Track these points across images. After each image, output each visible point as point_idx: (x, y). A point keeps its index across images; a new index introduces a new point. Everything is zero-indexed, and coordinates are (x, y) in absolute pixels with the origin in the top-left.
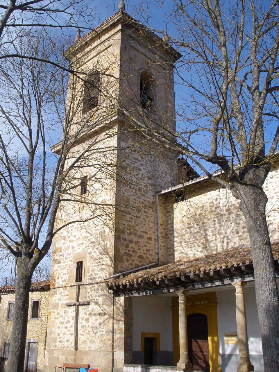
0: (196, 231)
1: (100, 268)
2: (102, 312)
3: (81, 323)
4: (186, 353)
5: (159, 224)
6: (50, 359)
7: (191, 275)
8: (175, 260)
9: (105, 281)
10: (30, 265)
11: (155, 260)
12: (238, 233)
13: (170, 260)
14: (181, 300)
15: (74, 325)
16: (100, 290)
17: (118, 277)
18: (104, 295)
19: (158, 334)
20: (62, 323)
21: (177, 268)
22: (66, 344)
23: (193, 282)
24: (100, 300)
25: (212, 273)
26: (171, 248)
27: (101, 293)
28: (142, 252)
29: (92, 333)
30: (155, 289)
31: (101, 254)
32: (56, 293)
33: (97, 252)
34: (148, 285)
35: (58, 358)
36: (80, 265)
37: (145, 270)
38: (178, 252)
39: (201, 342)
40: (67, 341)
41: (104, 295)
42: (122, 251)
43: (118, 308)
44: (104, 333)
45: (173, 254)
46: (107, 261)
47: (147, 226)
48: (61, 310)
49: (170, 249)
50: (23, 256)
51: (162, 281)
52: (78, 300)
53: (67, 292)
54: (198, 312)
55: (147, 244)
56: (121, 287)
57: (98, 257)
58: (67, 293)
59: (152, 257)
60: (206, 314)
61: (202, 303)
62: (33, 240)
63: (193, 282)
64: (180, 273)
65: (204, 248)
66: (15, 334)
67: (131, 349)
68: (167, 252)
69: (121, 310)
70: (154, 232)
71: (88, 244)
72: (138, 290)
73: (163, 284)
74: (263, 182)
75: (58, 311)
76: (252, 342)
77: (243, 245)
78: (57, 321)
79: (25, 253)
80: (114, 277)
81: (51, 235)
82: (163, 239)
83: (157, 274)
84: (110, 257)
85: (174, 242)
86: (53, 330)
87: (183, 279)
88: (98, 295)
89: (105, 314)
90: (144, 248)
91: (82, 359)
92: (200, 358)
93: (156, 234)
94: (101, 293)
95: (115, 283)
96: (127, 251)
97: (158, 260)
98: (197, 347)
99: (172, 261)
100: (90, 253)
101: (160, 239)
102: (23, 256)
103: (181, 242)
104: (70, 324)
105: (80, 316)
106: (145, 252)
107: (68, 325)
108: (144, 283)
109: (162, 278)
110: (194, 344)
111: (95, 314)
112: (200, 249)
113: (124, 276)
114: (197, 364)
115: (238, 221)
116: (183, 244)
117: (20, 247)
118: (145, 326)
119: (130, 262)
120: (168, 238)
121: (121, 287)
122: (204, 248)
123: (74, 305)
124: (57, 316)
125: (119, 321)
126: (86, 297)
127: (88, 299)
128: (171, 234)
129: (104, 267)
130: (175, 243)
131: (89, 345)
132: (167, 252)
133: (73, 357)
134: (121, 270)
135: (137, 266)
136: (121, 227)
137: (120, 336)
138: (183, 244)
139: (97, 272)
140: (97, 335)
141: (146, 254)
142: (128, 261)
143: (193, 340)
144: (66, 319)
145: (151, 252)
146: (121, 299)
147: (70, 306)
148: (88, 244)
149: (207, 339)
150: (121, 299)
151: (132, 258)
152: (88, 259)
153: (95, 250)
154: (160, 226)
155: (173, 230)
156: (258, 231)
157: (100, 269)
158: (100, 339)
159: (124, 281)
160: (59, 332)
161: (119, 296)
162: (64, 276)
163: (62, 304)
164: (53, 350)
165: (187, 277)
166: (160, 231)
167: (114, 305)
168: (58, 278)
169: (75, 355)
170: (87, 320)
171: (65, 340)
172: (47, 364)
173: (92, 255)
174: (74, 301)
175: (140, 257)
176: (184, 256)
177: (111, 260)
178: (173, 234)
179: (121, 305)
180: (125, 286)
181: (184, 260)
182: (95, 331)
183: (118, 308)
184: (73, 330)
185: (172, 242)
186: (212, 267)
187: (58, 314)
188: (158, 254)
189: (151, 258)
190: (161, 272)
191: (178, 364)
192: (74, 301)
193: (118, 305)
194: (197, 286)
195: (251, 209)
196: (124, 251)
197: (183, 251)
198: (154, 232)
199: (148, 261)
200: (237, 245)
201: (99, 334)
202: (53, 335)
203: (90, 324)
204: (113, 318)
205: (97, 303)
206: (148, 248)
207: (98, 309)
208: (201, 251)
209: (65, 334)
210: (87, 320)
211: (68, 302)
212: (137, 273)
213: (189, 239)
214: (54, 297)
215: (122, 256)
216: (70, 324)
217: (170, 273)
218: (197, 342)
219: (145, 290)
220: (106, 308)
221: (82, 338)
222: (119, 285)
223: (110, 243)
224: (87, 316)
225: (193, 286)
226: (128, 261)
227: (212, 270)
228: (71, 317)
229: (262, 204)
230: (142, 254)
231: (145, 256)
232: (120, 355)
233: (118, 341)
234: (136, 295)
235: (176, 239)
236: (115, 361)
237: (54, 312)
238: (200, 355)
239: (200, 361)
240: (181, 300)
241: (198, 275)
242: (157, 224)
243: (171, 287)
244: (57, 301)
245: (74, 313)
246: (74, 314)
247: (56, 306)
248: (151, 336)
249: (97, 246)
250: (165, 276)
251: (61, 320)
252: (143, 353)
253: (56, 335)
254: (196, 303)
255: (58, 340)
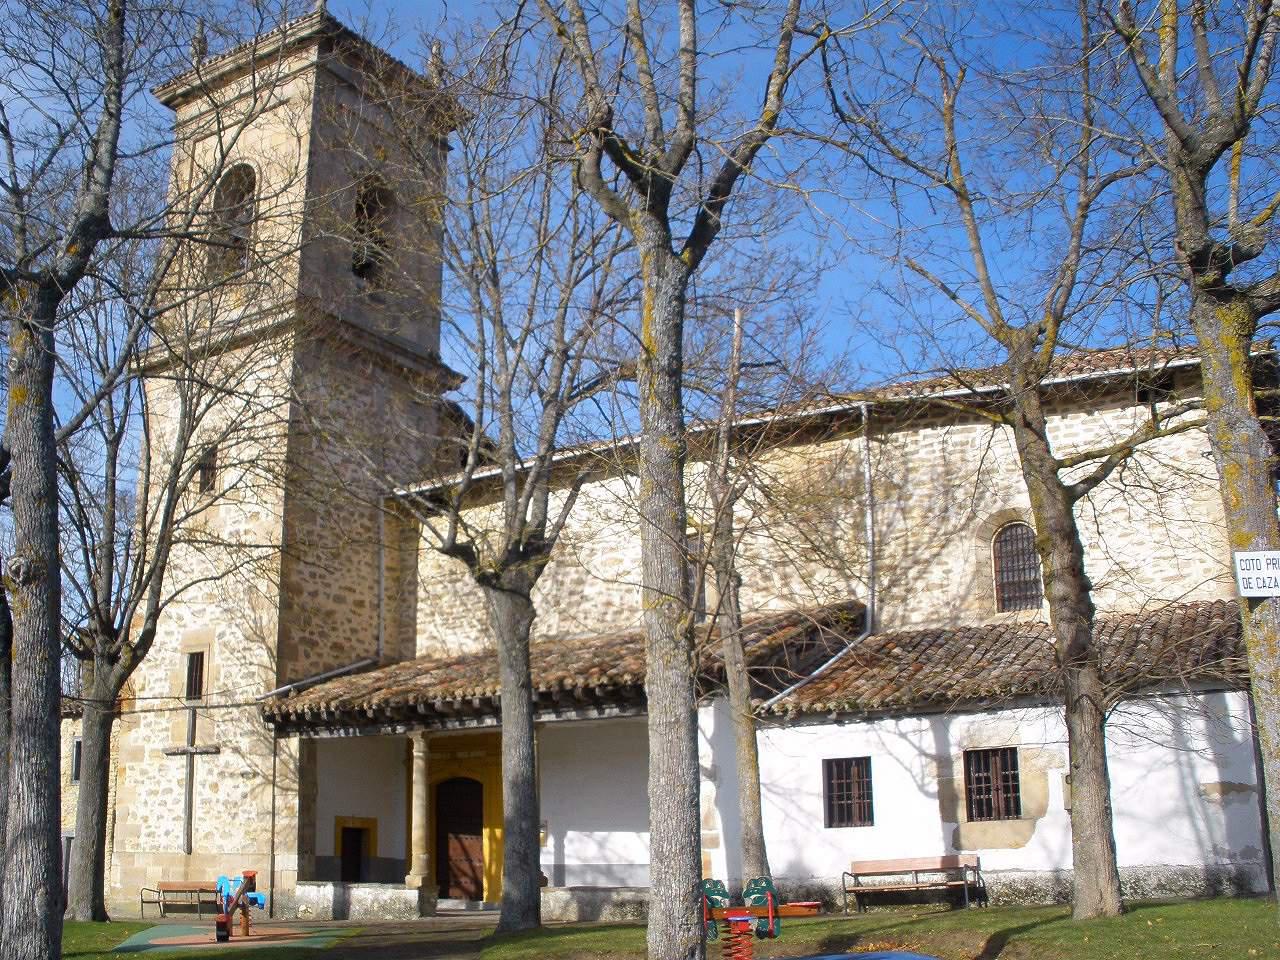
0: (467, 590)
1: (245, 671)
2: (248, 769)
3: (201, 794)
4: (423, 857)
5: (383, 567)
6: (125, 873)
7: (438, 703)
8: (418, 654)
9: (260, 704)
10: (113, 680)
11: (371, 654)
12: (557, 603)
13: (405, 653)
14: (418, 751)
15: (183, 798)
16: (244, 720)
17: (286, 694)
18: (253, 733)
19: (375, 821)
20: (155, 793)
21: (412, 682)
22: (163, 841)
23: (442, 716)
24: (245, 743)
25: (476, 702)
26: (409, 625)
27: (248, 727)
28: (341, 635)
29: (225, 816)
30: (366, 725)
31: (247, 638)
32: (136, 724)
33: (239, 634)
34: (349, 715)
35: (145, 872)
36: (196, 662)
37: (346, 679)
38: (426, 635)
39: (468, 840)
40: (167, 833)
41: (253, 733)
42: (296, 635)
43: (284, 762)
44: (253, 815)
45: (413, 640)
46: (262, 656)
47: (354, 574)
48: (150, 764)
49: (406, 628)
50: (97, 661)
51: (380, 710)
52: (192, 741)
53: (164, 722)
54: (463, 774)
55: (351, 616)
56: (293, 717)
57: (241, 646)
58: (164, 724)
59: (365, 646)
60: (477, 777)
61: (473, 754)
62: (116, 626)
63: (442, 716)
64: (416, 698)
65: (481, 631)
66: (85, 815)
67: (312, 851)
68: (400, 633)
69: (292, 766)
70: (371, 588)
71: (218, 615)
72: (329, 725)
73: (380, 717)
74: (531, 585)
75: (144, 765)
76: (571, 841)
77: (568, 633)
78: (141, 789)
79: (102, 656)
80: (277, 694)
81: (154, 614)
82: (394, 604)
83: (370, 688)
84: (269, 649)
85: (416, 610)
86: (132, 809)
87: (421, 709)
88: (239, 731)
89: (255, 774)
90: (347, 626)
91: (204, 872)
92: (465, 874)
93: (376, 591)
94: (248, 727)
95: (279, 708)
96: (307, 635)
97: (377, 653)
98: (459, 851)
99: (409, 654)
100: (221, 635)
101: (382, 604)
102: (97, 661)
103: (433, 614)
104: (174, 795)
105: (198, 777)
106: (348, 634)
107: (169, 798)
108: (343, 713)
109: (378, 705)
110: (453, 844)
111: (232, 775)
112: (474, 634)
113: (299, 690)
114: (458, 885)
115: (560, 578)
116: (437, 618)
117: (87, 640)
118: (344, 804)
119: (314, 658)
120: (404, 600)
121: (293, 717)
122: (481, 631)
123: (183, 753)
124: (140, 778)
125: (287, 790)
126: (210, 736)
127: (215, 741)
128: (410, 593)
129: (253, 669)
130: (419, 615)
131: (219, 841)
132: (400, 633)
133: (182, 869)
134: (293, 676)
135: (328, 668)
136: (294, 578)
137: (288, 823)
138: (437, 618)
139: (239, 680)
140: (237, 821)
141: (349, 640)
142: (307, 656)
143: (451, 835)
144: (164, 785)
145: (361, 635)
146: (293, 744)
147: (174, 754)
148: (218, 615)
149: (481, 834)
150: (293, 744)
151: (318, 650)
152: (216, 648)
153: (235, 629)
154: (386, 574)
155: (415, 584)
156: (511, 666)
157: (244, 672)
158: (243, 828)
159: (301, 704)
160: (148, 813)
161: (287, 736)
162: (159, 684)
163: (152, 751)
164: (132, 855)
165: (430, 706)
166: (384, 584)
167: (275, 755)
168: (143, 689)
169: (187, 865)
170: (215, 787)
171: (161, 831)
172: (118, 885)
173: (225, 639)
174: (184, 744)
175: (337, 647)
176: (439, 645)
177: (271, 655)
178: (414, 593)
179: (291, 756)
180: (301, 716)
181: (437, 656)
182: (234, 811)
183: (284, 762)
184: (181, 807)
185: (411, 611)
186: (479, 690)
187: (143, 772)
188: (377, 638)
189: (360, 649)
190: (379, 689)
191: (407, 878)
192: (184, 744)
193: (284, 756)
194: (450, 725)
195: (505, 631)
196: (301, 634)
197: (436, 634)
198: (371, 588)
199: (353, 655)
200: (553, 632)
201: (242, 817)
202: (130, 821)
203: (222, 796)
204: (274, 784)
205: (236, 750)
206: (354, 625)
207: (239, 764)
208: (477, 639)
209: (160, 817)
210: (215, 787)
211: (169, 744)
212: (328, 685)
213: (451, 607)
214: (133, 734)
215: (295, 648)
216: (174, 795)
217: (397, 694)
218: (460, 841)
219: (345, 726)
220: (257, 760)
221: (200, 827)
222: (288, 714)
223: (269, 618)
224: (214, 778)
225: (444, 724)
226: (307, 656)
227: (478, 695)
228: (175, 781)
229: (525, 622)
230: (341, 640)
231: (347, 645)
232: (288, 862)
233: (284, 834)
234: (325, 735)
235: (420, 605)
236: (277, 876)
237: (132, 769)
238: (465, 866)
239: (463, 880)
240: (418, 751)
241: (450, 704)
242: (379, 568)
243: (399, 722)
244: (140, 743)
245: (184, 770)
246: (183, 774)
247: (137, 754)
248: (358, 825)
249: (238, 621)
250: (387, 701)
251: (149, 786)
252: (338, 862)
253: (139, 821)
254: (460, 755)
255: (144, 831)
